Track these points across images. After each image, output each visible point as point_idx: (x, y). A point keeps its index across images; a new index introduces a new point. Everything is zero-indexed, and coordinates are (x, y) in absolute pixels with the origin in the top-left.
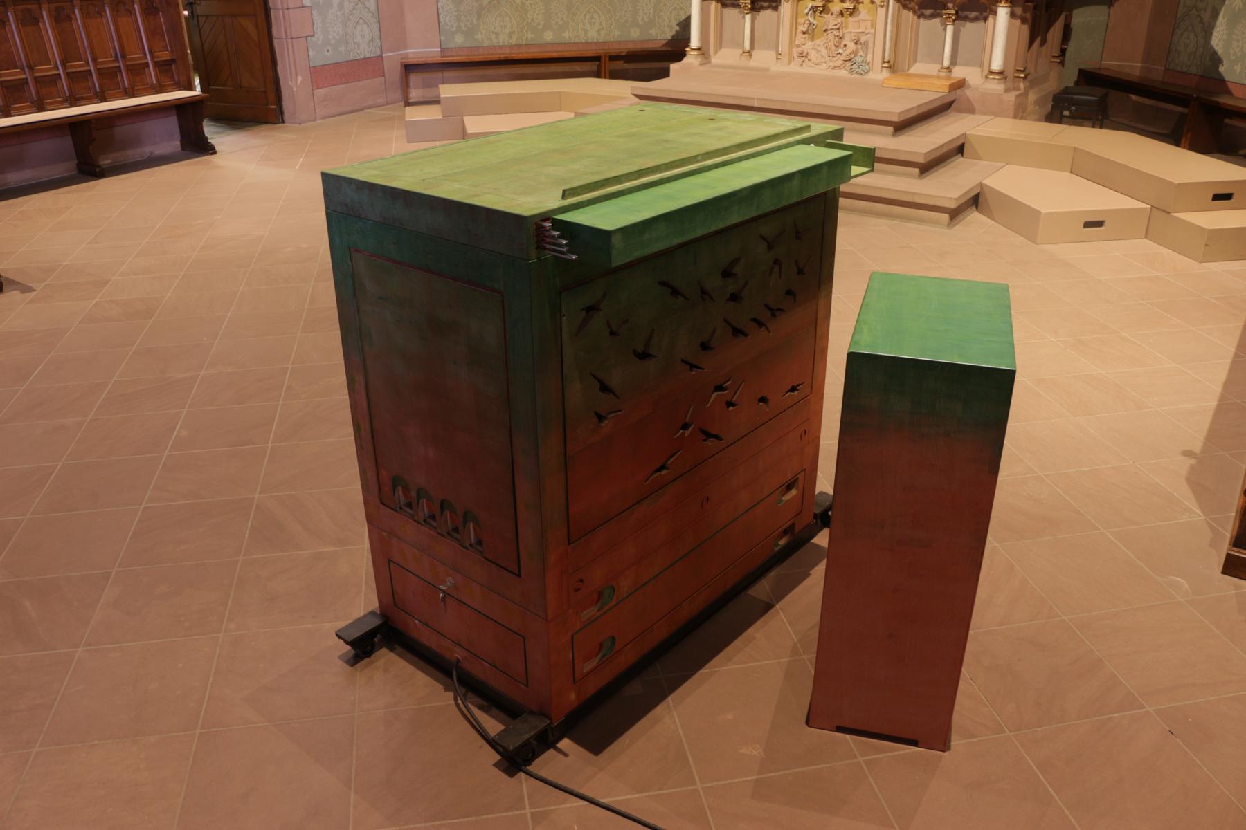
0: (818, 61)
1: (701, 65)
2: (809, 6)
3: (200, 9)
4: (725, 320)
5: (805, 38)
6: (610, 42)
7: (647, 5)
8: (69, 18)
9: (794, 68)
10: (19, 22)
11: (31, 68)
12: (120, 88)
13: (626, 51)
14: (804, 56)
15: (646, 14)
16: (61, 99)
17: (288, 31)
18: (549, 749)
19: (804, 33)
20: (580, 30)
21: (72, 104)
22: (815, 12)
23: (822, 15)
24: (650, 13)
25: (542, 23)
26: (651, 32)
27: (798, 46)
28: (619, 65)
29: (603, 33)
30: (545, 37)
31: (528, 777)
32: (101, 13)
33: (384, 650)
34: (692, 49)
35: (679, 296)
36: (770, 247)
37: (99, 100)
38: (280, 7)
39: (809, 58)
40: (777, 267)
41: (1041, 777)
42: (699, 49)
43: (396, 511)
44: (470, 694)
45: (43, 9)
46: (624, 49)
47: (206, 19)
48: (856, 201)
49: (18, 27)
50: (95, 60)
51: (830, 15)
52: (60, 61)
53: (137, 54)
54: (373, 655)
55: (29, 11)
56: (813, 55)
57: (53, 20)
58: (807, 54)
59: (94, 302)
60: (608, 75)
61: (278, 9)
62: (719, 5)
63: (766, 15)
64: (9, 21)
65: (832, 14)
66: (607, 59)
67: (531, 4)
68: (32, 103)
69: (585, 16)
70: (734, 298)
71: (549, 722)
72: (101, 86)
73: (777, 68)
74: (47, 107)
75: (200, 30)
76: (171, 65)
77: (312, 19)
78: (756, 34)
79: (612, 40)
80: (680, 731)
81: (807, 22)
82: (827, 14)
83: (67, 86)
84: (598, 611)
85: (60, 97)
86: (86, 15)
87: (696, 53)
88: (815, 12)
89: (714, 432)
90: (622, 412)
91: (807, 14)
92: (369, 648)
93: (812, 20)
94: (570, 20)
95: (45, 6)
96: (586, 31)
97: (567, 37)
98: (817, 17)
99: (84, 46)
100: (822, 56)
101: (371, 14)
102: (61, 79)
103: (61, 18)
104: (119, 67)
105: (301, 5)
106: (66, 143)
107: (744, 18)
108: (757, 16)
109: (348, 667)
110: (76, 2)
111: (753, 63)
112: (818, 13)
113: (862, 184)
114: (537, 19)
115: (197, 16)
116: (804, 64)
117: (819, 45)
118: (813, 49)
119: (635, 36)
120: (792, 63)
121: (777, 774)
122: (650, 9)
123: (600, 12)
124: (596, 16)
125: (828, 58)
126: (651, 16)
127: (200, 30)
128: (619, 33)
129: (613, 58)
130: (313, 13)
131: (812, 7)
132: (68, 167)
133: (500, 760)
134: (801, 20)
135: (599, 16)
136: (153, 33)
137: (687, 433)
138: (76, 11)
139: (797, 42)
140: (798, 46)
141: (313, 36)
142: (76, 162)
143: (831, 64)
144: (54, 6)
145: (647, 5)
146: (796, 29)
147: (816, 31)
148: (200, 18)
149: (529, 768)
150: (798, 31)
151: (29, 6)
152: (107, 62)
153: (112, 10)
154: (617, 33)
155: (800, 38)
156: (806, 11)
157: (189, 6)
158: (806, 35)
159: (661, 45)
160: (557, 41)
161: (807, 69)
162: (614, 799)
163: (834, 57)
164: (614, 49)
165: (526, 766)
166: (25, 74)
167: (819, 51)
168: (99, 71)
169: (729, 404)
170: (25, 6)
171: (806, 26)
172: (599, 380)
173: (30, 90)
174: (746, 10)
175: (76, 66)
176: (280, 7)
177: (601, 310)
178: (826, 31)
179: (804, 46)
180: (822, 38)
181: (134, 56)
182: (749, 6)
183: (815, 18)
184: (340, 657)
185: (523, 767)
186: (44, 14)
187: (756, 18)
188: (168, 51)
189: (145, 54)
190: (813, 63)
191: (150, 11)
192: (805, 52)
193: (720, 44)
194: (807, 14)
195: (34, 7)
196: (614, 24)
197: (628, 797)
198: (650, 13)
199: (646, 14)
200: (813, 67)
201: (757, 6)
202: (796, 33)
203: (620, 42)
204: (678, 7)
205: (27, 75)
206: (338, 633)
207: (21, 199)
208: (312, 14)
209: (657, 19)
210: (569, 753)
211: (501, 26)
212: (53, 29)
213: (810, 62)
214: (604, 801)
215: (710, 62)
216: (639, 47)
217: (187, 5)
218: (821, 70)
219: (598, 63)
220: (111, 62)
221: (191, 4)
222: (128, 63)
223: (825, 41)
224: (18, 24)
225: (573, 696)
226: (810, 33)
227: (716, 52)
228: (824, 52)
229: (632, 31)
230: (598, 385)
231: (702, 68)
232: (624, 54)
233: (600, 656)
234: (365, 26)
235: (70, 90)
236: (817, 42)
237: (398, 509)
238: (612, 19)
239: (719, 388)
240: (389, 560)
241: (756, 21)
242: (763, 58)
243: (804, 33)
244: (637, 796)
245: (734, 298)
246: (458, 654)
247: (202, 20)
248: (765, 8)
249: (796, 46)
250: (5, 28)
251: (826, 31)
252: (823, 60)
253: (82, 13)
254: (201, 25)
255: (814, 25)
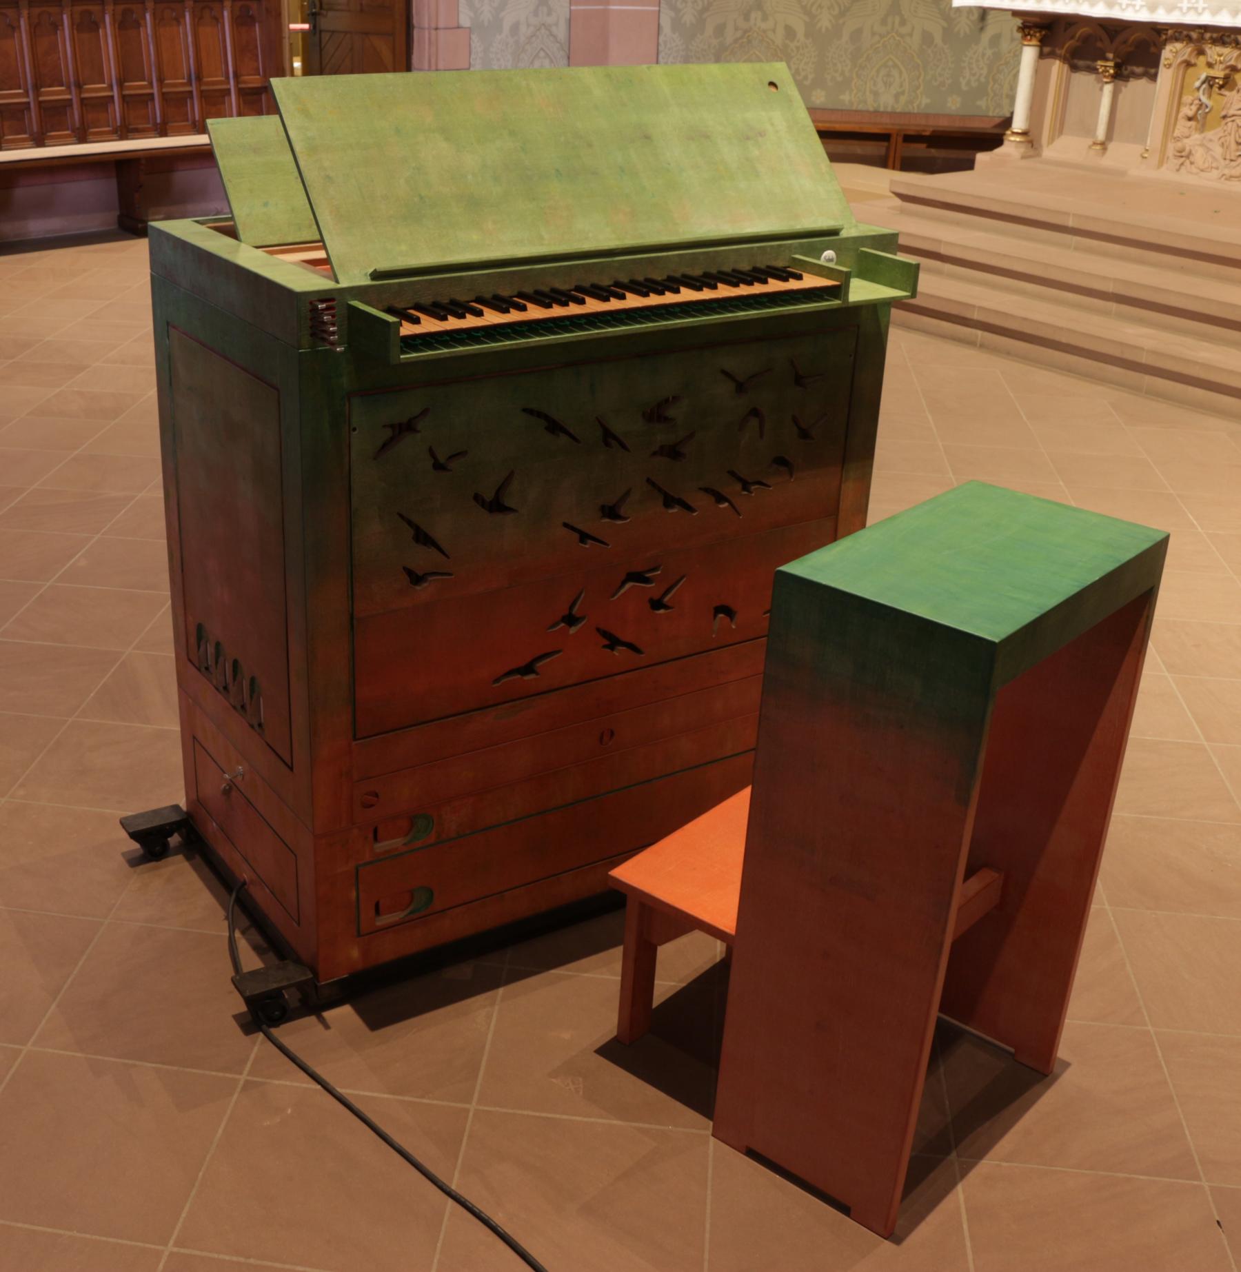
0: (1206, 165)
1: (1023, 157)
2: (1203, 77)
3: (326, 23)
4: (648, 480)
5: (1190, 128)
6: (914, 114)
7: (977, 61)
8: (138, 24)
9: (1167, 173)
10: (75, 27)
11: (79, 86)
12: (187, 120)
13: (931, 129)
14: (1184, 155)
15: (974, 75)
16: (110, 129)
17: (433, 61)
18: (309, 1014)
19: (1190, 119)
20: (868, 93)
21: (123, 137)
22: (1211, 86)
23: (1223, 91)
24: (981, 75)
25: (811, 77)
26: (979, 103)
27: (1178, 139)
28: (920, 150)
29: (903, 99)
30: (813, 98)
31: (266, 1039)
32: (178, 20)
33: (180, 857)
34: (1014, 133)
35: (561, 434)
36: (741, 388)
37: (158, 134)
38: (426, 26)
39: (1192, 159)
40: (754, 422)
41: (965, 1226)
42: (1024, 134)
43: (199, 670)
44: (253, 931)
45: (107, 12)
46: (928, 126)
47: (331, 36)
48: (1190, 388)
49: (73, 32)
50: (161, 81)
51: (1234, 92)
52: (116, 79)
53: (216, 76)
54: (163, 861)
55: (90, 13)
56: (1199, 155)
57: (117, 26)
58: (1190, 153)
59: (58, 390)
60: (898, 164)
61: (423, 29)
62: (1066, 67)
63: (1137, 86)
64: (62, 25)
65: (1238, 91)
66: (900, 139)
67: (798, 48)
68: (73, 131)
69: (878, 71)
70: (673, 452)
71: (311, 976)
72: (164, 115)
73: (1139, 171)
74: (91, 138)
75: (321, 50)
76: (261, 94)
77: (470, 45)
78: (1119, 115)
79: (916, 111)
80: (490, 1036)
81: (1197, 102)
82: (1231, 89)
83: (120, 112)
84: (405, 844)
85: (109, 126)
86: (159, 21)
87: (1018, 139)
88: (1211, 86)
89: (627, 637)
90: (453, 577)
91: (1198, 89)
92: (157, 848)
93: (1204, 99)
94: (854, 76)
95: (110, 8)
96: (876, 94)
97: (984, 108)
98: (1214, 96)
99: (150, 61)
100: (1213, 157)
101: (558, 45)
102: (113, 102)
103: (126, 25)
104: (191, 92)
105: (456, 25)
106: (102, 188)
107: (1101, 89)
108: (1123, 89)
109: (126, 866)
110: (150, 5)
111: (1111, 159)
112: (1215, 89)
113: (1200, 361)
114: (803, 70)
115: (321, 31)
116: (1183, 169)
117: (1211, 140)
118: (1202, 145)
119: (954, 108)
120: (1165, 166)
121: (585, 1119)
122: (982, 69)
123: (903, 70)
124: (895, 73)
125: (1222, 161)
126: (983, 79)
127: (321, 50)
128: (928, 101)
129: (909, 138)
130: (473, 37)
131: (1207, 77)
132: (105, 219)
133: (244, 1013)
134: (1187, 98)
135: (901, 73)
136: (242, 50)
137: (573, 630)
138: (148, 16)
139: (1177, 133)
140: (1178, 139)
141: (469, 69)
142: (118, 213)
143: (1226, 172)
144: (121, 7)
145: (977, 61)
146: (1178, 111)
147: (1209, 116)
148: (323, 34)
149: (275, 1032)
150: (1181, 115)
151: (90, 8)
152: (177, 84)
153: (193, 16)
154: (925, 101)
155: (1182, 127)
156: (1197, 84)
157: (311, 16)
158: (1192, 123)
159: (992, 124)
160: (830, 106)
161: (1187, 177)
162: (356, 1092)
163: (1232, 160)
164: (913, 127)
165: (270, 1026)
166: (70, 93)
167: (1211, 150)
168: (164, 96)
169: (657, 604)
170: (85, 7)
171: (1194, 108)
172: (410, 523)
173: (73, 114)
174: (1105, 77)
175: (136, 86)
176: (426, 26)
177: (418, 432)
178: (1224, 117)
179: (1186, 141)
180: (1219, 129)
181: (214, 79)
182: (1112, 71)
183: (1210, 97)
184: (123, 854)
185: (264, 1027)
186: (108, 19)
187: (1120, 91)
188: (259, 75)
189: (228, 77)
190: (1199, 168)
191: (243, 20)
192: (1188, 149)
193: (1060, 128)
194: (1198, 89)
195: (95, 8)
196: (922, 88)
197: (376, 1095)
198: (981, 75)
199: (974, 75)
200: (1197, 174)
201: (1126, 73)
202: (1176, 119)
203: (927, 116)
204: (890, 63)
205: (72, 96)
206: (123, 821)
207: (36, 254)
208: (470, 38)
209: (991, 83)
210: (331, 1025)
211: (885, 83)
212: (115, 37)
213: (1193, 166)
214: (340, 1090)
215: (1039, 155)
216: (957, 125)
217: (308, 15)
218: (1210, 181)
219: (886, 144)
220: (182, 85)
221: (314, 14)
222: (203, 88)
223: (1222, 134)
224: (73, 29)
225: (355, 953)
226: (1200, 119)
227: (1052, 140)
228: (1218, 151)
229: (950, 99)
230: (411, 532)
231: (1024, 163)
232: (928, 133)
233: (406, 912)
234: (547, 62)
235: (123, 118)
236: (1209, 134)
237: (203, 669)
238: (921, 80)
239: (638, 577)
240: (194, 738)
241: (1121, 97)
242: (1122, 155)
243: (1190, 119)
244: (386, 1096)
245: (673, 452)
246: (245, 874)
247: (325, 37)
248: (1138, 76)
249: (1175, 138)
250: (56, 33)
251: (1224, 117)
252: (1214, 165)
253: (155, 19)
254: (323, 45)
255: (1207, 107)
